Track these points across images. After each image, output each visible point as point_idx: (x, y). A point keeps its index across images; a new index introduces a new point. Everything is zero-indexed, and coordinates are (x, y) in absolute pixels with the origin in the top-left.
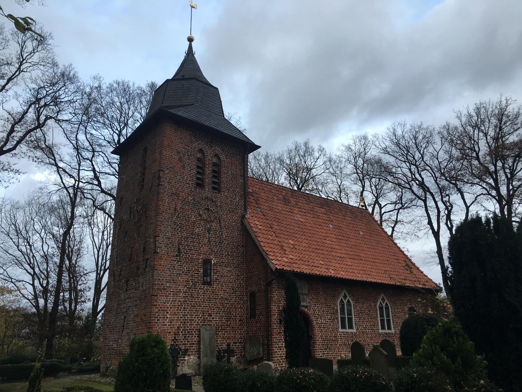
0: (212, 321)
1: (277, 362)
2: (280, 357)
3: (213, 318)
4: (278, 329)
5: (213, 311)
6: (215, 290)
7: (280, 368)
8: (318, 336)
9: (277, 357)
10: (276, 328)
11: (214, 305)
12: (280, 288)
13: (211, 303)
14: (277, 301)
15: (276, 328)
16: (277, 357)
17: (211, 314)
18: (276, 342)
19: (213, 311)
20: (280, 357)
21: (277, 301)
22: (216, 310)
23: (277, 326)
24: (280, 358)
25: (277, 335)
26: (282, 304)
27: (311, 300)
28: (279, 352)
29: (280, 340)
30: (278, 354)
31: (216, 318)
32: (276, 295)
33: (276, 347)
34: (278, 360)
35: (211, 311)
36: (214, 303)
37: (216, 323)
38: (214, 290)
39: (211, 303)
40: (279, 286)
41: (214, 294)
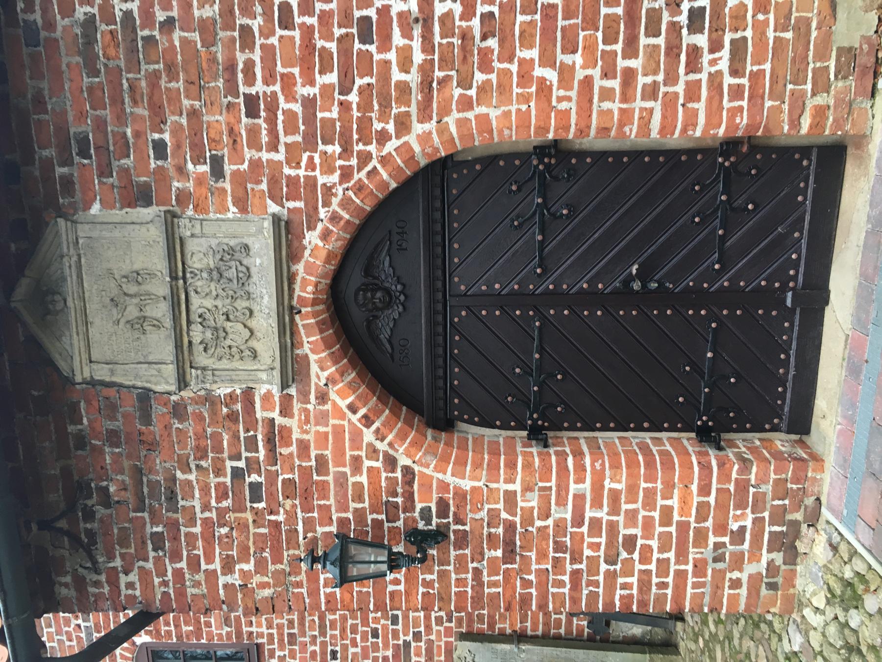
0: (430, 643)
1: (719, 575)
2: (681, 556)
3: (417, 636)
4: (479, 555)
5: (386, 637)
6: (280, 627)
7: (765, 557)
8: (544, 88)
9: (681, 575)
10: (477, 572)
11: (354, 630)
12: (174, 526)
13: (345, 648)
14: (277, 559)
15: (477, 572)
16: (681, 575)
17: (396, 647)
18: (576, 575)
19: (386, 637)
20: (681, 556)
21: (277, 559)
22: (376, 620)
23: (461, 564)
24: (693, 553)
25: (525, 567)
26: (291, 516)
27: (217, 171)
28: (645, 559)
29: (559, 547)
30: (663, 564)
31: (416, 624)
32: (228, 566)
33: (611, 577)
34: (700, 568)
35: (386, 646)
36: (343, 630)
37: (439, 621)
38: (281, 635)
39: (345, 648)
40: (158, 541)
41: (304, 634)
